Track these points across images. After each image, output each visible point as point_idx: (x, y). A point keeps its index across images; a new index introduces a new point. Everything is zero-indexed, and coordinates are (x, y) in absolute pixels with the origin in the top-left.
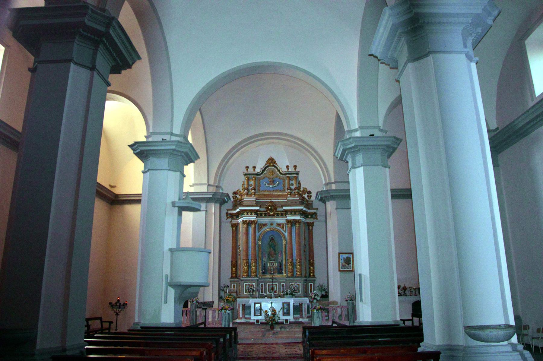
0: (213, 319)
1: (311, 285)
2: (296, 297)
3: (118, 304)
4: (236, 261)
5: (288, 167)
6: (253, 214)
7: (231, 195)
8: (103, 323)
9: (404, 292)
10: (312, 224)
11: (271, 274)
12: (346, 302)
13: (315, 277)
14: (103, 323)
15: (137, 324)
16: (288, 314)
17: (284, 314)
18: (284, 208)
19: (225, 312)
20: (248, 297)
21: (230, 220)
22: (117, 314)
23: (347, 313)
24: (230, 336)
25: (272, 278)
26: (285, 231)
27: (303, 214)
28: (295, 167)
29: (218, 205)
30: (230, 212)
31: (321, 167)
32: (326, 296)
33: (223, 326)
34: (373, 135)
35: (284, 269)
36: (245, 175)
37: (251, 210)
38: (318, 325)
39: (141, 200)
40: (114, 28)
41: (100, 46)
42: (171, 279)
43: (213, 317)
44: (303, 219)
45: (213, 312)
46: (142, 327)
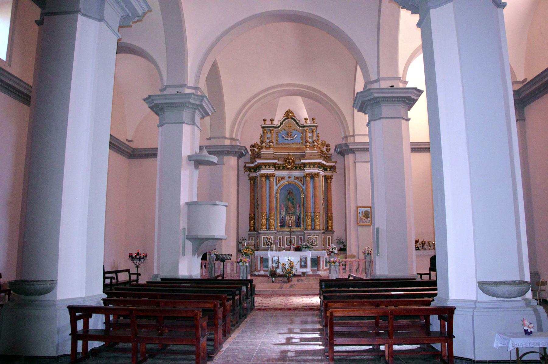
0: (230, 271)
1: (329, 238)
2: (314, 250)
5: (306, 119)
6: (271, 167)
7: (249, 149)
8: (131, 275)
9: (423, 246)
10: (331, 178)
11: (289, 227)
12: (364, 256)
14: (131, 275)
15: (157, 276)
16: (305, 266)
17: (301, 267)
18: (303, 161)
20: (267, 250)
21: (248, 173)
22: (137, 267)
23: (364, 267)
24: (247, 288)
25: (291, 231)
27: (325, 168)
28: (313, 119)
29: (236, 158)
30: (247, 165)
32: (343, 250)
33: (241, 278)
34: (393, 87)
35: (302, 222)
36: (263, 127)
37: (269, 163)
43: (232, 270)
44: (322, 173)
45: (232, 264)
46: (162, 279)
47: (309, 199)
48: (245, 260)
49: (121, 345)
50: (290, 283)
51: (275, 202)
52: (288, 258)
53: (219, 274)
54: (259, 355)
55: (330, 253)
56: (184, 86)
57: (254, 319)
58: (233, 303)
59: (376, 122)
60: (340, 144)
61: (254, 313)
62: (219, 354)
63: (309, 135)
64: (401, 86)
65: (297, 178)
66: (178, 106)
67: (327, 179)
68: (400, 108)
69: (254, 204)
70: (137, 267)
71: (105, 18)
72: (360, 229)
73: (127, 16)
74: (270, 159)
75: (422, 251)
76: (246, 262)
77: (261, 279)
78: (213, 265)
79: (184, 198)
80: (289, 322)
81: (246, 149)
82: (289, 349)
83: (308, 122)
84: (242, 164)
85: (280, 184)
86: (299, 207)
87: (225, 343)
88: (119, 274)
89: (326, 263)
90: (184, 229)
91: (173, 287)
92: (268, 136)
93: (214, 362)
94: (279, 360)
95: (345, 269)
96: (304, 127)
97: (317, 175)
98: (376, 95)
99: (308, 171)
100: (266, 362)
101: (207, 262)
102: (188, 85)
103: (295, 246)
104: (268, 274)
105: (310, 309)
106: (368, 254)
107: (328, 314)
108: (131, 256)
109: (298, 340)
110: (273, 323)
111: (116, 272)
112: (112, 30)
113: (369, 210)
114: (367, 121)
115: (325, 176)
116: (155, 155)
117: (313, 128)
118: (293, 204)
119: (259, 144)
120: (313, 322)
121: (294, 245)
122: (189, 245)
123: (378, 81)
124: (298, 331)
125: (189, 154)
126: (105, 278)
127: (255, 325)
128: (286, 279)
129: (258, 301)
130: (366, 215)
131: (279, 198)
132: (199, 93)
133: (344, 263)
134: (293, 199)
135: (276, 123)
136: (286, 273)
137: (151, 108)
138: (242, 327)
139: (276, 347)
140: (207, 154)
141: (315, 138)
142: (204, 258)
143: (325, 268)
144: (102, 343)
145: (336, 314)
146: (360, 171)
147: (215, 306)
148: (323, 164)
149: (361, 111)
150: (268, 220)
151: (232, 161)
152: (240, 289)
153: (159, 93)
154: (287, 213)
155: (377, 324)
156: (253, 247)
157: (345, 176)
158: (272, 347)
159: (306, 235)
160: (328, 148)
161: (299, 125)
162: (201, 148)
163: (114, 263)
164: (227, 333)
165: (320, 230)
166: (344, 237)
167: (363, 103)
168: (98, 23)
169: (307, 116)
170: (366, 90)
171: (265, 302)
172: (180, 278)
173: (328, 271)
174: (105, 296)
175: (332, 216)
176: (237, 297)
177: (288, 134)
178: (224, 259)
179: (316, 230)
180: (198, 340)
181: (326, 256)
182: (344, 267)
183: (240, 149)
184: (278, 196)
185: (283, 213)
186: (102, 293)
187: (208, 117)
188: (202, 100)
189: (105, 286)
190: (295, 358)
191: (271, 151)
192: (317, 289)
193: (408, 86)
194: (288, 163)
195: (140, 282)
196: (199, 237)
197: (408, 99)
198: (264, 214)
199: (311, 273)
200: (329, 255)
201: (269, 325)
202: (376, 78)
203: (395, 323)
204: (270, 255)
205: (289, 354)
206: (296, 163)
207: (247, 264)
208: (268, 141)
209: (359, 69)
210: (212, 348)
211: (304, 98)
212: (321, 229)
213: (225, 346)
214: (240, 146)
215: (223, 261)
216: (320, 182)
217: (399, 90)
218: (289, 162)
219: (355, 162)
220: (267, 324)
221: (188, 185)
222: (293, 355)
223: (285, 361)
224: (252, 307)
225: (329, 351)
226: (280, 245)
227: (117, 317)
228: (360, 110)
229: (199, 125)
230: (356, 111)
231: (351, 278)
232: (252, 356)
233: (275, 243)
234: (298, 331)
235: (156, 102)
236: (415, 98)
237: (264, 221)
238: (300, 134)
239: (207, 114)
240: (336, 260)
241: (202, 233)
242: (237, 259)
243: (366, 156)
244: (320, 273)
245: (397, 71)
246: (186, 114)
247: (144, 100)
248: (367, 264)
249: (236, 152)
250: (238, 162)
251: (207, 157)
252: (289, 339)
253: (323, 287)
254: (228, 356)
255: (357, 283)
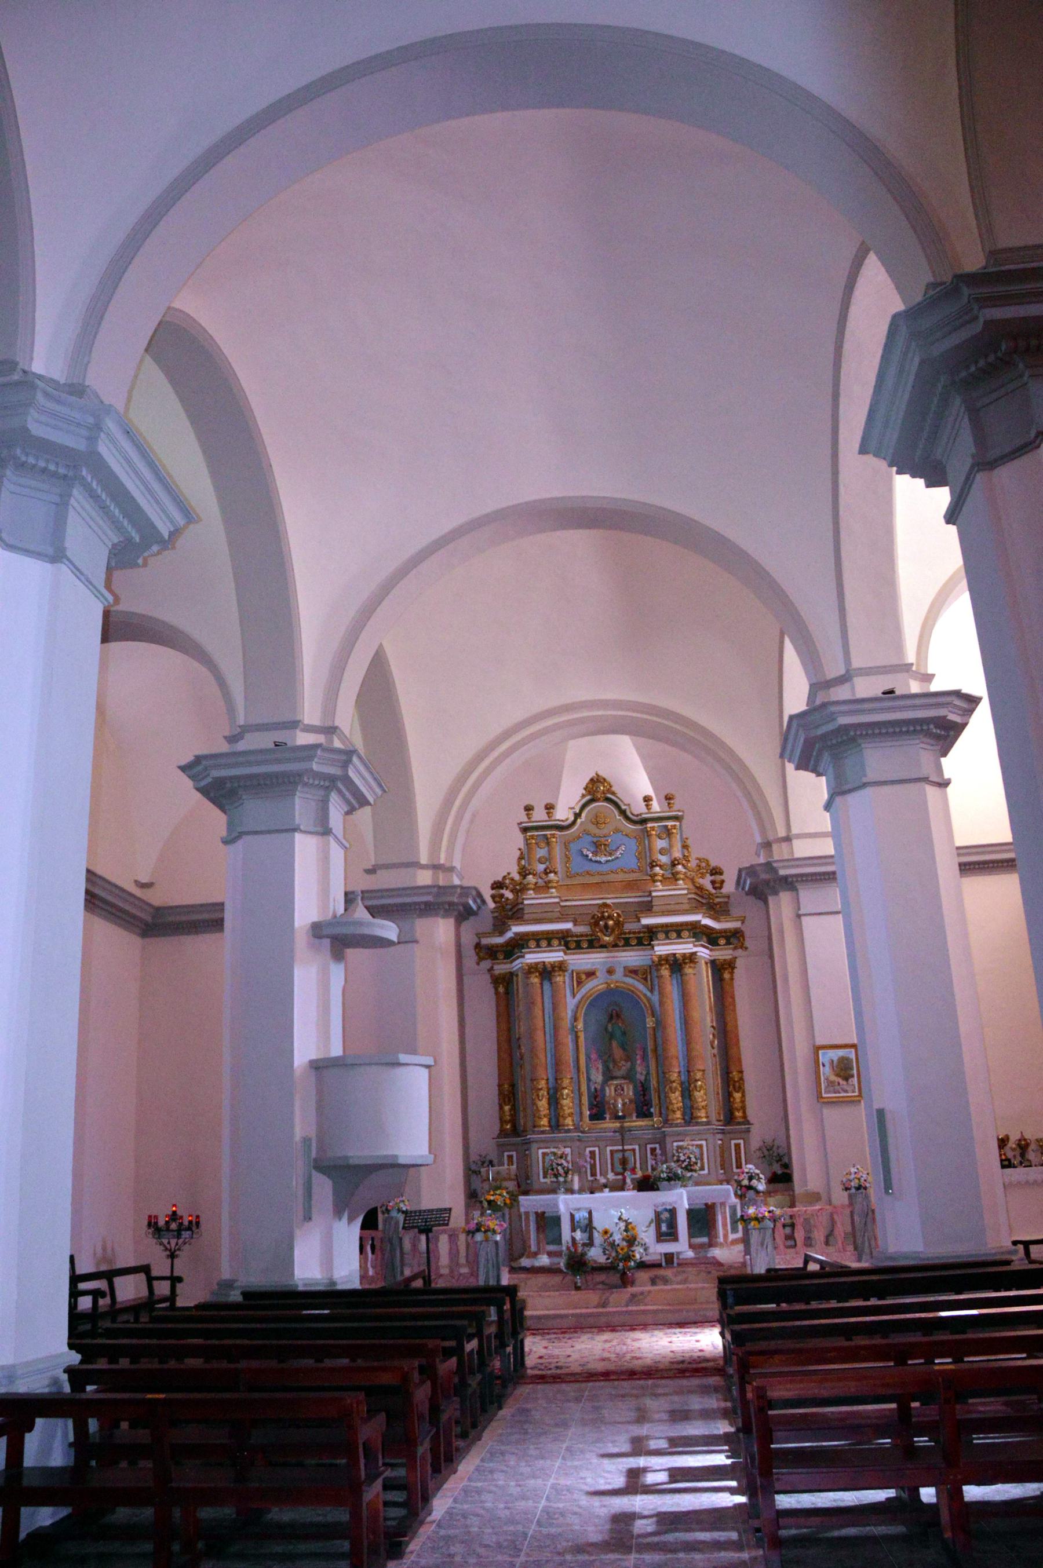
0: (449, 1262)
1: (737, 1146)
2: (697, 1184)
3: (174, 1226)
4: (513, 1086)
5: (647, 799)
6: (555, 942)
7: (487, 893)
8: (155, 1283)
9: (1022, 1155)
10: (730, 965)
11: (617, 1118)
12: (846, 1194)
13: (749, 1123)
14: (155, 1283)
15: (229, 1285)
16: (672, 1235)
17: (660, 1237)
18: (645, 921)
19: (487, 1240)
20: (554, 1191)
21: (486, 964)
22: (172, 1256)
23: (849, 1229)
24: (500, 1313)
25: (622, 1131)
26: (652, 991)
27: (711, 938)
28: (668, 798)
29: (451, 922)
30: (485, 941)
31: (498, 761)
32: (782, 1178)
33: (481, 1283)
34: (892, 692)
35: (655, 1101)
36: (525, 830)
37: (548, 932)
38: (763, 1271)
39: (222, 920)
40: (113, 441)
41: (75, 492)
42: (321, 1148)
43: (454, 1254)
44: (704, 953)
45: (453, 1237)
46: (246, 1295)
47: (670, 1031)
48: (492, 1224)
49: (122, 1514)
50: (631, 1290)
51: (571, 1046)
52: (618, 1212)
53: (416, 1270)
54: (545, 1531)
55: (745, 1191)
56: (294, 725)
57: (525, 1411)
58: (460, 1363)
59: (852, 799)
60: (752, 866)
61: (524, 1390)
62: (421, 1530)
63: (660, 844)
64: (915, 687)
65: (632, 972)
66: (277, 783)
67: (720, 970)
68: (920, 751)
69: (511, 1055)
70: (172, 1256)
71: (68, 554)
72: (827, 1111)
73: (129, 540)
74: (551, 921)
75: (1021, 1170)
76: (494, 1232)
77: (542, 1279)
78: (396, 1242)
79: (305, 1048)
80: (633, 1415)
81: (479, 895)
82: (637, 1510)
83: (656, 806)
84: (469, 939)
85: (584, 991)
86: (644, 1058)
87: (439, 1494)
88: (118, 1281)
89: (734, 1222)
90: (306, 1141)
91: (280, 1310)
92: (541, 852)
93: (408, 1560)
94: (606, 1546)
95: (790, 1237)
96: (644, 821)
97: (692, 958)
98: (844, 720)
99: (662, 949)
100: (568, 1557)
101: (378, 1235)
102: (306, 722)
103: (639, 1174)
104: (562, 1263)
105: (697, 1370)
106: (858, 1188)
107: (749, 1395)
108: (152, 1223)
109: (662, 1477)
110: (584, 1423)
111: (109, 1275)
112: (89, 583)
113: (851, 1054)
114: (826, 796)
115: (713, 963)
116: (217, 925)
117: (670, 823)
118: (624, 1049)
119: (517, 877)
120: (706, 1415)
121: (633, 1171)
122: (324, 1188)
123: (844, 679)
124: (663, 1444)
125: (316, 919)
126: (75, 1294)
127: (530, 1428)
128: (615, 1279)
129: (536, 1349)
130: (844, 1070)
131: (582, 1035)
132: (337, 744)
133: (788, 1221)
134: (624, 1033)
135: (563, 814)
136: (616, 1258)
137: (204, 791)
138: (489, 1439)
139: (596, 1501)
140: (366, 916)
141: (677, 854)
142: (370, 1222)
143: (732, 1237)
144: (64, 1512)
145: (777, 1392)
146: (818, 944)
147: (405, 1378)
148: (706, 926)
149: (806, 769)
150: (554, 1100)
151: (441, 931)
152: (479, 1319)
153: (224, 748)
154: (608, 1076)
155: (904, 1411)
156: (511, 1185)
157: (771, 957)
158: (584, 1501)
159: (668, 1140)
160: (718, 878)
161: (627, 818)
162: (349, 898)
163: (104, 1249)
164: (444, 1461)
165: (708, 1123)
166: (781, 1141)
167: (809, 745)
168: (48, 566)
169: (650, 791)
170: (816, 710)
171: (556, 1352)
172: (301, 1288)
173: (741, 1247)
174: (75, 1358)
175: (742, 1079)
176: (472, 1345)
177: (598, 846)
178: (427, 1223)
179: (697, 1124)
180: (356, 1489)
181: (734, 1200)
182: (788, 1230)
183: (461, 895)
184: (580, 1026)
185: (598, 1077)
186: (66, 1348)
187: (367, 809)
188: (346, 764)
189: (75, 1317)
190: (656, 1539)
191: (551, 898)
192: (714, 1309)
193: (935, 687)
194: (602, 931)
195: (180, 1303)
196: (351, 1162)
197: (939, 724)
198: (542, 1084)
199: (690, 1254)
200: (741, 1197)
201: (573, 1429)
202: (842, 672)
203: (960, 1412)
204: (566, 1204)
205: (641, 1526)
206: (629, 927)
207: (498, 1238)
208: (541, 867)
209: (788, 645)
210: (401, 1512)
211: (641, 740)
212: (713, 1118)
213: (440, 1506)
214: (462, 887)
215: (427, 1231)
216: (701, 979)
217: (909, 702)
218: (606, 926)
219: (799, 916)
220: (565, 1425)
221: (316, 1012)
222: (650, 1529)
223: (627, 1549)
224: (517, 1372)
225: (758, 1522)
226: (593, 1174)
227: (109, 1425)
228: (803, 765)
229: (339, 833)
230: (790, 767)
231: (813, 1267)
232: (525, 1535)
233: (578, 1170)
234: (663, 1444)
235: (216, 773)
236: (958, 719)
237: (543, 1104)
238: (633, 844)
239: (363, 802)
240: (764, 1211)
241: (359, 1152)
242: (467, 1222)
243: (831, 896)
244: (717, 1253)
245: (899, 646)
246: (302, 806)
247: (183, 769)
248: (856, 1217)
249: (451, 904)
250: (458, 936)
251: (369, 924)
252: (634, 1474)
253: (730, 1300)
254: (448, 1540)
255: (835, 1282)
